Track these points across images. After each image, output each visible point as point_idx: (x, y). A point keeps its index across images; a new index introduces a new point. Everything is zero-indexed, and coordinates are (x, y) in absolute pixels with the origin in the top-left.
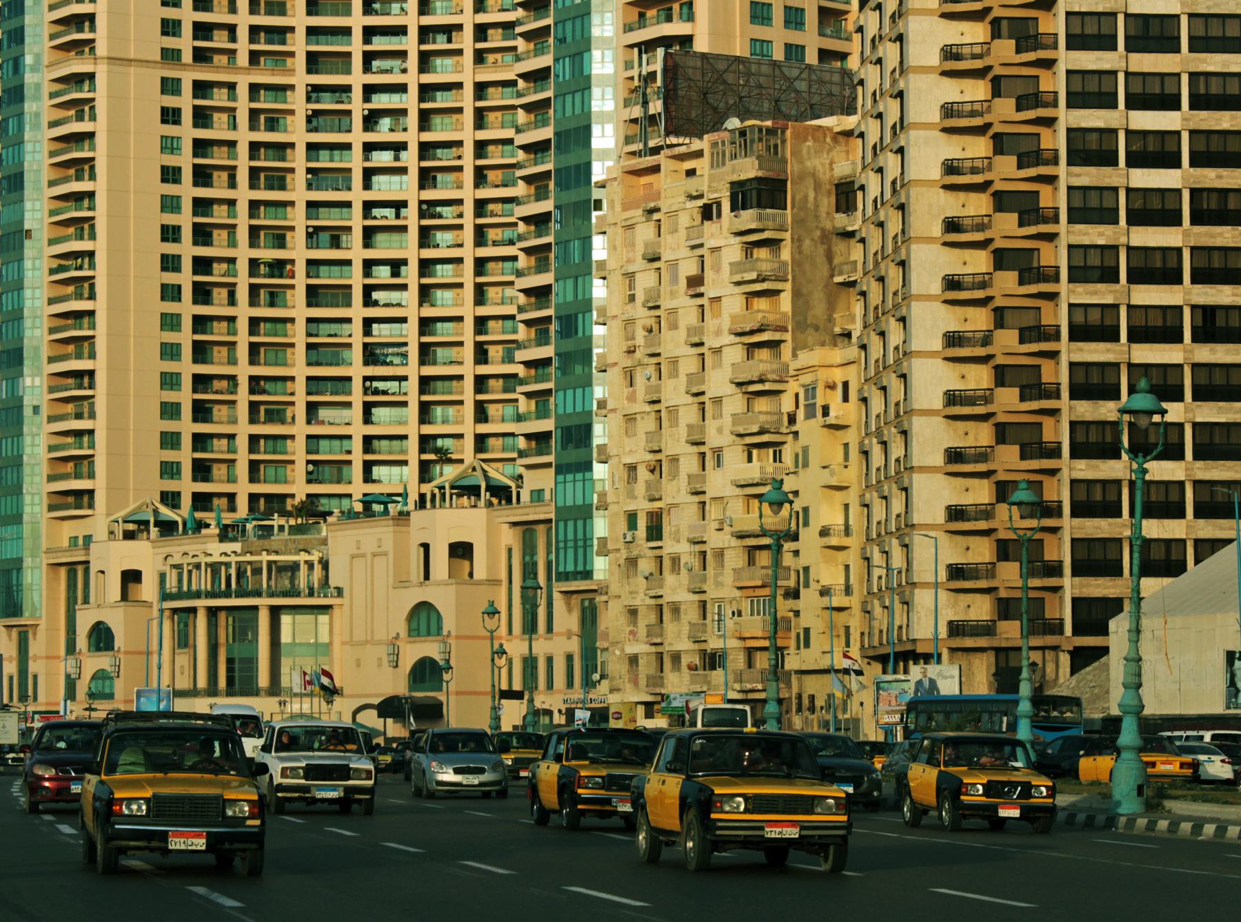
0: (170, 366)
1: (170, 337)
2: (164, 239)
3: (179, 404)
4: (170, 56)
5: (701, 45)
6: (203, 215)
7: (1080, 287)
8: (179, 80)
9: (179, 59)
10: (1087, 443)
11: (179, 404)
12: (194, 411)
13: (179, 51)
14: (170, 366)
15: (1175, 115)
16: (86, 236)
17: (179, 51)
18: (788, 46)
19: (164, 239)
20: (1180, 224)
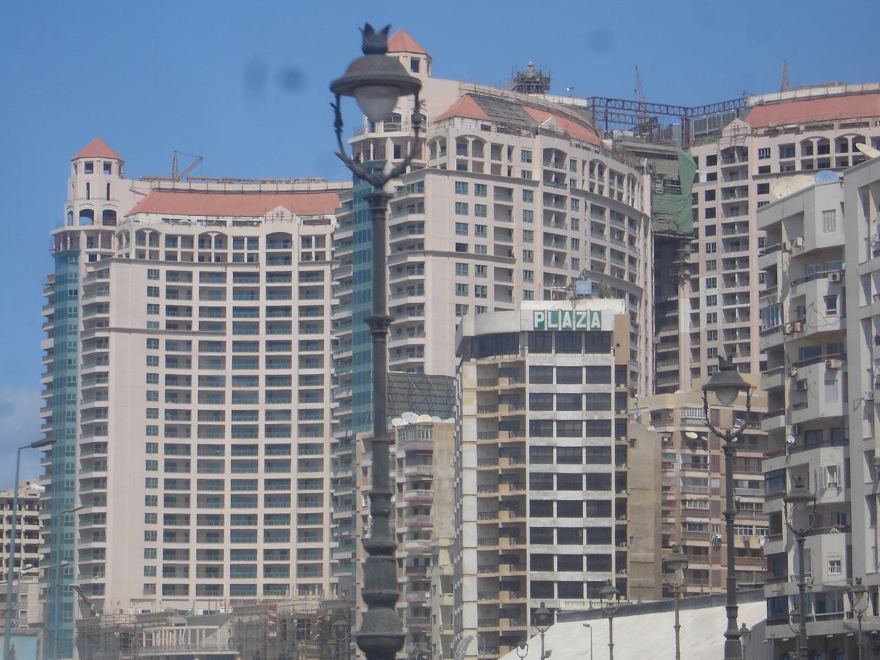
0: (152, 439)
1: (152, 387)
2: (147, 486)
3: (157, 462)
4: (153, 325)
5: (429, 370)
6: (172, 454)
7: (534, 492)
8: (158, 340)
9: (158, 258)
10: (511, 618)
11: (157, 462)
12: (165, 466)
13: (158, 323)
14: (152, 439)
15: (579, 439)
16: (99, 581)
17: (158, 323)
18: (477, 246)
19: (147, 486)
20: (581, 383)
